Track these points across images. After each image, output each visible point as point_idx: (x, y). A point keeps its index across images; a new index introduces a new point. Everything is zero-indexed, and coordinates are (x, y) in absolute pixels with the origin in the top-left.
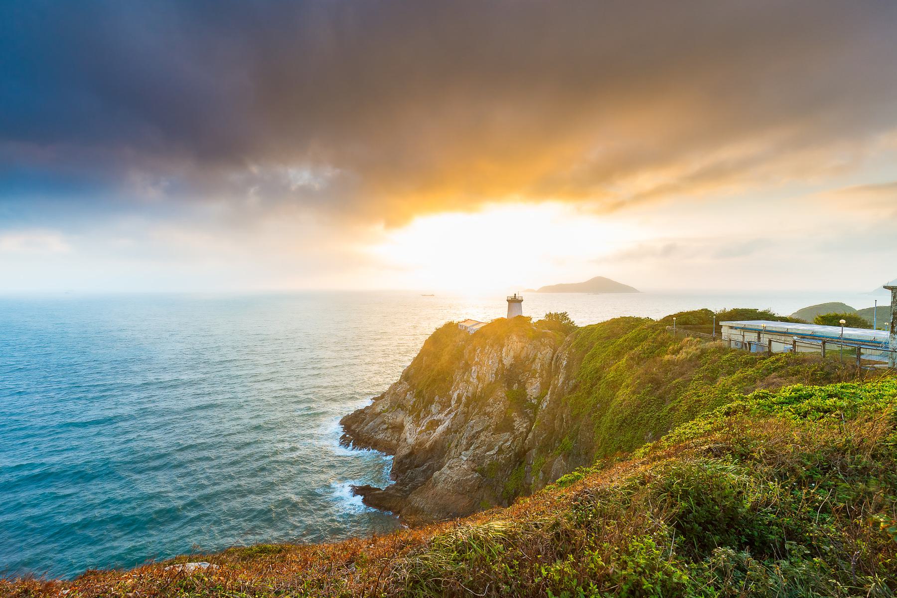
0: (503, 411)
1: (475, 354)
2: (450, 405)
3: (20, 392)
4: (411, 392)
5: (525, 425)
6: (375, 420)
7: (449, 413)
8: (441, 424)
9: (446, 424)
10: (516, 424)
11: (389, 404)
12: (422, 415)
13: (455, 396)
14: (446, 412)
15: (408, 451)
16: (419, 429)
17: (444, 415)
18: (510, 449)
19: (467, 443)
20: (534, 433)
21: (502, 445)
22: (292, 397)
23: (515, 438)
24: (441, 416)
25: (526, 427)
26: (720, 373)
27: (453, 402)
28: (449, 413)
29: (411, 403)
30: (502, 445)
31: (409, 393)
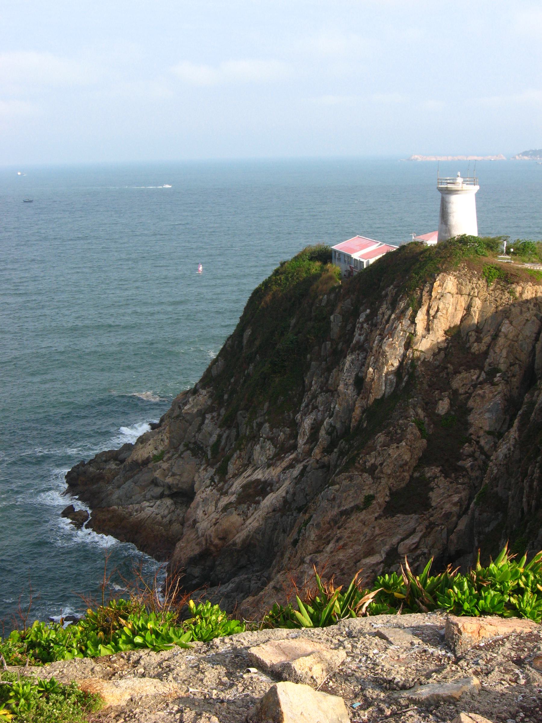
0: (406, 464)
1: (354, 326)
2: (294, 447)
3: (110, 326)
4: (215, 414)
5: (456, 498)
6: (136, 477)
7: (291, 466)
8: (272, 491)
9: (281, 492)
10: (435, 497)
11: (167, 441)
12: (231, 468)
13: (307, 423)
14: (284, 464)
15: (197, 550)
16: (225, 501)
17: (279, 469)
18: (419, 552)
19: (319, 537)
20: (473, 518)
21: (398, 543)
22: (100, 404)
23: (431, 527)
24: (273, 473)
25: (459, 503)
26: (82, 517)
27: (301, 441)
28: (291, 466)
29: (214, 438)
30: (398, 543)
31: (208, 416)
